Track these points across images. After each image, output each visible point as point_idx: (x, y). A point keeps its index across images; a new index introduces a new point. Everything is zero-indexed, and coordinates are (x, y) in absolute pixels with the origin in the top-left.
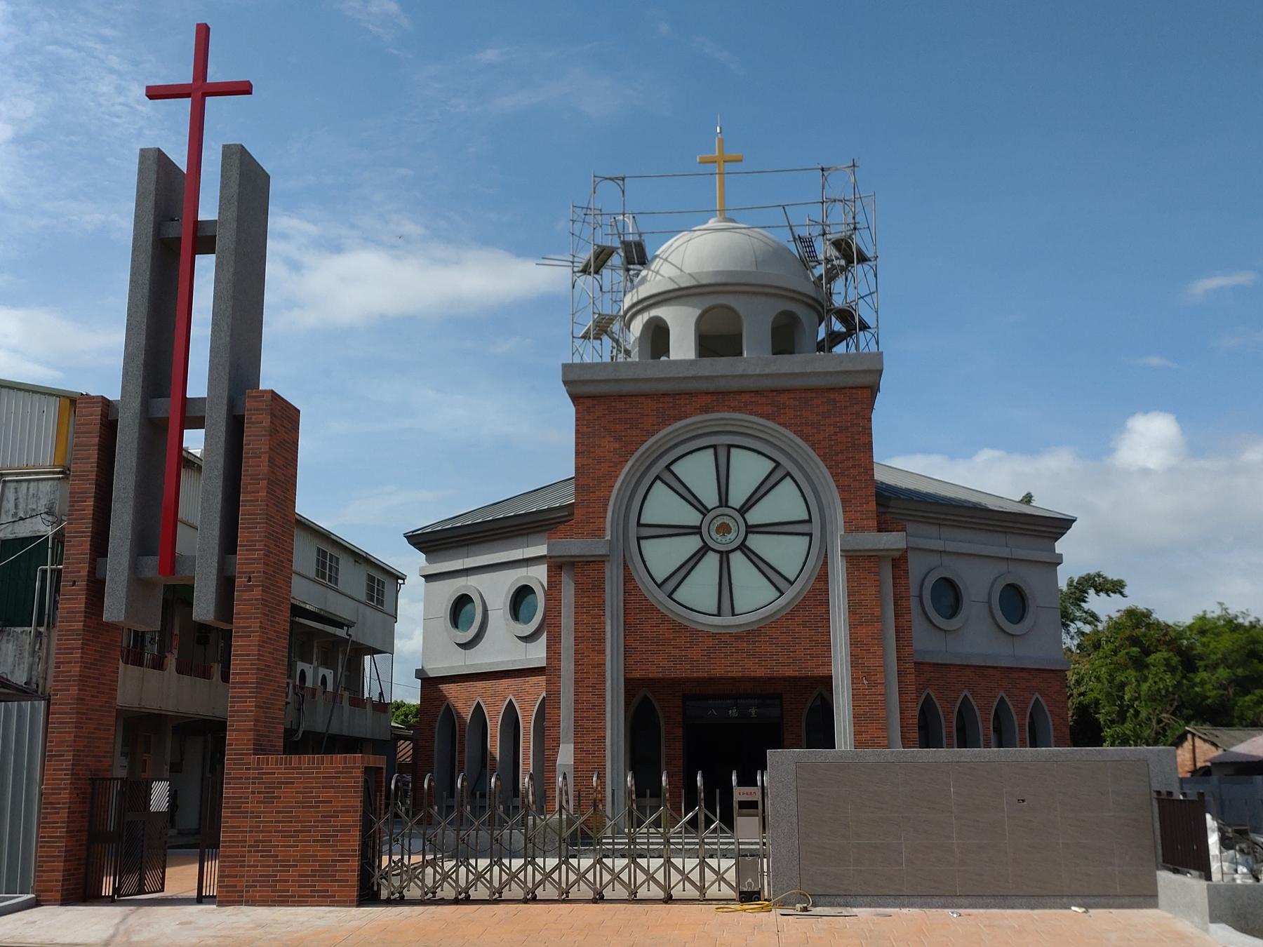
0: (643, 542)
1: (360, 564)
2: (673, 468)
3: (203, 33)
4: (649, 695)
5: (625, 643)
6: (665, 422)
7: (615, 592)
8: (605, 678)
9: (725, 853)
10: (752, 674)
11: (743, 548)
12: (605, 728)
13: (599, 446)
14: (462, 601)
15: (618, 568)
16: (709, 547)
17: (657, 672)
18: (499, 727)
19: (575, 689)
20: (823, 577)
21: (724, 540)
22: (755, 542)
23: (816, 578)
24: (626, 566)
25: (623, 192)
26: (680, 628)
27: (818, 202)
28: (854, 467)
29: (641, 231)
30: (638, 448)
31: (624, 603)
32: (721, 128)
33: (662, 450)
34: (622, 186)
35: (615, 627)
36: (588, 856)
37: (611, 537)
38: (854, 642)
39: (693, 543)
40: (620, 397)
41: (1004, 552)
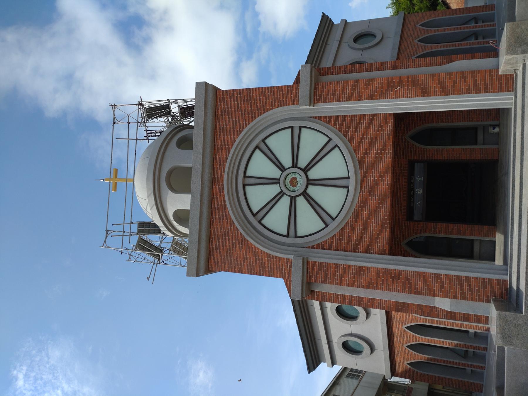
1: (339, 382)
4: (406, 241)
5: (364, 253)
6: (228, 215)
8: (387, 269)
10: (390, 166)
11: (305, 170)
13: (237, 257)
14: (346, 346)
16: (304, 191)
17: (386, 232)
19: (394, 292)
20: (327, 119)
21: (300, 182)
22: (303, 162)
23: (328, 124)
24: (313, 247)
25: (114, 231)
26: (356, 215)
28: (260, 99)
30: (240, 232)
31: (337, 251)
32: (101, 179)
33: (243, 218)
34: (111, 232)
37: (292, 255)
38: (371, 97)
39: (301, 202)
40: (210, 241)
41: (336, 44)
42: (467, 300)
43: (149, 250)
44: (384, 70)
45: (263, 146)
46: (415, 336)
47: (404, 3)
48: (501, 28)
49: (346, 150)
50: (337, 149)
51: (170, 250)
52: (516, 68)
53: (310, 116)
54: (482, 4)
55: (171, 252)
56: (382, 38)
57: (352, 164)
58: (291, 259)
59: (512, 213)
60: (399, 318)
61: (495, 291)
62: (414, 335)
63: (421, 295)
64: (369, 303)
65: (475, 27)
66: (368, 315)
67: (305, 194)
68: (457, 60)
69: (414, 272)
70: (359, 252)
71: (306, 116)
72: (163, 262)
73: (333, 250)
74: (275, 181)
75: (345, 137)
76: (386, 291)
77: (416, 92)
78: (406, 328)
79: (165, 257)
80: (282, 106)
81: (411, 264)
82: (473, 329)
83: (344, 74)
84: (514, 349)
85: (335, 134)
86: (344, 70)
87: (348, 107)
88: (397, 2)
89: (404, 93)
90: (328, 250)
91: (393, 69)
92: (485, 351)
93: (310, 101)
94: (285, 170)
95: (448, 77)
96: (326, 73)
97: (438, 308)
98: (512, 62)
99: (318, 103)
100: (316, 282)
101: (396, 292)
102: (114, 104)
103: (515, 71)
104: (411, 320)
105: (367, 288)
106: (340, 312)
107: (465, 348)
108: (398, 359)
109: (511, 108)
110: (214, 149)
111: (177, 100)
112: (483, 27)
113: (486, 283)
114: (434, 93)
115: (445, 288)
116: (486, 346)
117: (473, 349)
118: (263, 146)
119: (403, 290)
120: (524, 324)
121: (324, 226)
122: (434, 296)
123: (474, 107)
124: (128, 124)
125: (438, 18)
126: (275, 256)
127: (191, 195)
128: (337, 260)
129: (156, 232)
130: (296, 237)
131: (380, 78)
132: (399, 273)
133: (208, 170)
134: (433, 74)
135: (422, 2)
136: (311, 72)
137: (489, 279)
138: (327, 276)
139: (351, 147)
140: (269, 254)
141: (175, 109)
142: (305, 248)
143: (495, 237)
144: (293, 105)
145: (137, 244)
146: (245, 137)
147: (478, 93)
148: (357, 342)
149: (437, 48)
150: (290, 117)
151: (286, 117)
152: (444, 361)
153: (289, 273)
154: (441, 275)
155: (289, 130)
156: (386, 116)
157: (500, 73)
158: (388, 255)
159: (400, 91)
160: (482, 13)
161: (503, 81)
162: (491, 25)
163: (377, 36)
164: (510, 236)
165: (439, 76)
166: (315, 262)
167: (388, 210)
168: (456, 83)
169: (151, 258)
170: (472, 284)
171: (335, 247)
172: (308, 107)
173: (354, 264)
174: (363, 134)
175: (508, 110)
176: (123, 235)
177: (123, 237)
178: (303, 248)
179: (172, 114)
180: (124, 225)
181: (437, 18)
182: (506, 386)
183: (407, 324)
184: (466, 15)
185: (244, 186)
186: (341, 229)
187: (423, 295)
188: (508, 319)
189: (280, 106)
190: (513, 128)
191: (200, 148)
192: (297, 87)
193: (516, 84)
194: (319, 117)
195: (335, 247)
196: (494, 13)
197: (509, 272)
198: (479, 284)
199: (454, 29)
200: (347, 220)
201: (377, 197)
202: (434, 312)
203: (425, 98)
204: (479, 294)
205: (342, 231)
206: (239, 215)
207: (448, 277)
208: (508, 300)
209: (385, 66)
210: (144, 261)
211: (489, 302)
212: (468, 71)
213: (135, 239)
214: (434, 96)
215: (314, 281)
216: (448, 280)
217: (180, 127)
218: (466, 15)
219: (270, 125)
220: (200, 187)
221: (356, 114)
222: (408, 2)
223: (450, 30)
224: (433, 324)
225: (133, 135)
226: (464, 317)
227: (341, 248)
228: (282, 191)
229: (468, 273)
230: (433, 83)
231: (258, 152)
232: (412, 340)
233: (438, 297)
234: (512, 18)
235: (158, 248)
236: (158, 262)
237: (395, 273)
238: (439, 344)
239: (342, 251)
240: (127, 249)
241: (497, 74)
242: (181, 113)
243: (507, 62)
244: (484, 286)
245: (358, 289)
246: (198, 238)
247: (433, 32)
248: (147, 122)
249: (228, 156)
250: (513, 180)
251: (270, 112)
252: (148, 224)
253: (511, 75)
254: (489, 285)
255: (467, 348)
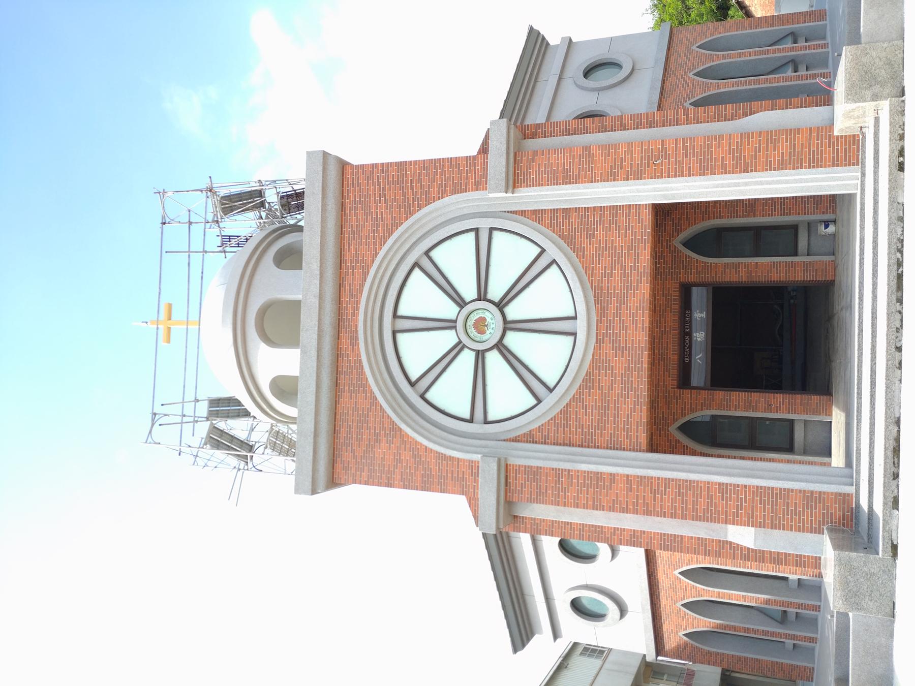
0: (491, 418)
2: (413, 378)
3: (193, 435)
5: (604, 448)
6: (365, 385)
7: (542, 455)
8: (645, 477)
9: (895, 329)
10: (647, 297)
11: (501, 305)
12: (708, 482)
13: (383, 459)
14: (577, 606)
15: (516, 449)
18: (709, 589)
19: (658, 516)
20: (537, 216)
21: (492, 326)
22: (496, 291)
24: (515, 440)
25: (165, 415)
26: (589, 382)
27: (189, 227)
28: (420, 181)
29: (194, 399)
30: (388, 416)
35: (584, 458)
36: (894, 528)
38: (612, 176)
39: (494, 359)
40: (334, 431)
41: (553, 81)
42: (784, 529)
43: (229, 448)
44: (634, 129)
45: (425, 263)
46: (696, 587)
47: (672, 5)
48: (836, 54)
49: (571, 269)
50: (554, 267)
51: (266, 448)
52: (862, 125)
53: (507, 210)
54: (805, 8)
55: (268, 451)
56: (633, 70)
57: (581, 293)
58: (478, 462)
59: (858, 376)
60: (668, 557)
61: (832, 514)
62: (693, 586)
63: (704, 521)
64: (614, 535)
65: (792, 49)
66: (614, 552)
67: (500, 346)
68: (761, 111)
69: (690, 481)
70: (595, 448)
71: (501, 210)
72: (254, 467)
73: (551, 444)
74: (449, 324)
75: (568, 246)
76: (644, 514)
77: (690, 167)
78: (680, 573)
79: (257, 458)
80: (458, 193)
81: (686, 467)
82: (796, 574)
83: (566, 135)
84: (866, 617)
85: (551, 241)
86: (566, 130)
87: (573, 194)
88: (660, 4)
89: (669, 168)
90: (542, 444)
91: (650, 127)
92: (816, 611)
93: (507, 184)
94: (466, 304)
95: (745, 141)
96: (534, 135)
97: (734, 543)
98: (856, 114)
99: (521, 187)
100: (522, 501)
101: (661, 516)
102: (164, 190)
103: (861, 129)
104: (689, 560)
105: (610, 511)
106: (565, 548)
107: (783, 606)
108: (666, 627)
109: (855, 194)
110: (341, 269)
111: (275, 181)
112: (806, 50)
113: (816, 500)
114: (722, 169)
115: (745, 509)
116: (818, 603)
117: (796, 608)
118: (425, 263)
119: (672, 513)
120: (881, 572)
121: (534, 402)
122: (726, 523)
123: (792, 193)
124: (187, 224)
125: (729, 34)
126: (450, 457)
127: (301, 350)
128: (557, 463)
129: (241, 414)
130: (486, 422)
131: (629, 143)
132: (665, 484)
133: (329, 306)
134: (719, 136)
135: (702, 3)
136: (508, 132)
137: (820, 492)
138: (540, 491)
139: (579, 263)
140: (439, 453)
141: (271, 197)
142: (501, 440)
143: (830, 415)
144: (477, 190)
145: (206, 437)
146: (395, 248)
147: (798, 168)
148: (595, 600)
149: (727, 87)
150: (474, 212)
151: (466, 212)
152: (746, 630)
153: (475, 486)
154: (738, 486)
155: (472, 235)
156: (639, 209)
157: (836, 133)
158: (647, 452)
159: (662, 166)
160: (804, 25)
161: (841, 146)
162: (819, 46)
163: (624, 66)
164: (855, 418)
165: (730, 139)
166: (519, 465)
167: (645, 374)
168: (760, 152)
169: (234, 461)
170: (792, 502)
171: (554, 438)
172: (504, 195)
173: (586, 469)
174: (600, 240)
175: (850, 198)
176: (182, 423)
177: (182, 426)
178: (499, 440)
179: (267, 205)
180: (183, 405)
181: (726, 34)
182: (852, 681)
183: (682, 567)
184: (777, 28)
185: (394, 333)
186: (564, 407)
187: (708, 521)
188: (855, 564)
189: (454, 192)
190: (858, 228)
191: (316, 266)
192: (484, 160)
193: (864, 152)
194: (522, 211)
195: (554, 438)
196: (826, 24)
197: (854, 480)
198: (804, 501)
199: (756, 53)
200: (575, 391)
201: (626, 351)
202: (727, 551)
203: (706, 177)
204: (803, 519)
205: (565, 412)
206: (386, 385)
207: (750, 490)
208: (854, 528)
209: (637, 122)
210: (220, 465)
211: (821, 532)
212: (779, 130)
213: (203, 428)
214: (722, 173)
215: (518, 500)
216: (749, 496)
217: (281, 229)
218: (777, 28)
219: (437, 226)
220: (316, 337)
221: (587, 206)
222: (679, 3)
223: (748, 56)
224: (726, 565)
225: (197, 245)
226: (779, 559)
227: (564, 441)
228: (460, 342)
229: (783, 482)
230: (719, 151)
231: (417, 272)
232: (691, 594)
233: (734, 524)
234: (855, 38)
235: (245, 443)
236: (246, 468)
237: (658, 483)
238: (737, 600)
239: (567, 445)
240: (189, 446)
241: (830, 135)
242: (282, 206)
243: (848, 115)
244: (812, 505)
245: (595, 512)
246: (313, 426)
247: (720, 59)
248: (221, 222)
249: (365, 281)
250: (859, 319)
251: (438, 203)
252: (226, 401)
253: (854, 136)
254: (820, 503)
255: (785, 607)
